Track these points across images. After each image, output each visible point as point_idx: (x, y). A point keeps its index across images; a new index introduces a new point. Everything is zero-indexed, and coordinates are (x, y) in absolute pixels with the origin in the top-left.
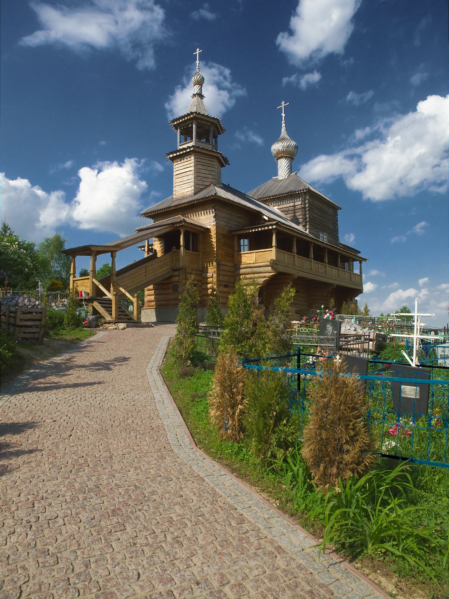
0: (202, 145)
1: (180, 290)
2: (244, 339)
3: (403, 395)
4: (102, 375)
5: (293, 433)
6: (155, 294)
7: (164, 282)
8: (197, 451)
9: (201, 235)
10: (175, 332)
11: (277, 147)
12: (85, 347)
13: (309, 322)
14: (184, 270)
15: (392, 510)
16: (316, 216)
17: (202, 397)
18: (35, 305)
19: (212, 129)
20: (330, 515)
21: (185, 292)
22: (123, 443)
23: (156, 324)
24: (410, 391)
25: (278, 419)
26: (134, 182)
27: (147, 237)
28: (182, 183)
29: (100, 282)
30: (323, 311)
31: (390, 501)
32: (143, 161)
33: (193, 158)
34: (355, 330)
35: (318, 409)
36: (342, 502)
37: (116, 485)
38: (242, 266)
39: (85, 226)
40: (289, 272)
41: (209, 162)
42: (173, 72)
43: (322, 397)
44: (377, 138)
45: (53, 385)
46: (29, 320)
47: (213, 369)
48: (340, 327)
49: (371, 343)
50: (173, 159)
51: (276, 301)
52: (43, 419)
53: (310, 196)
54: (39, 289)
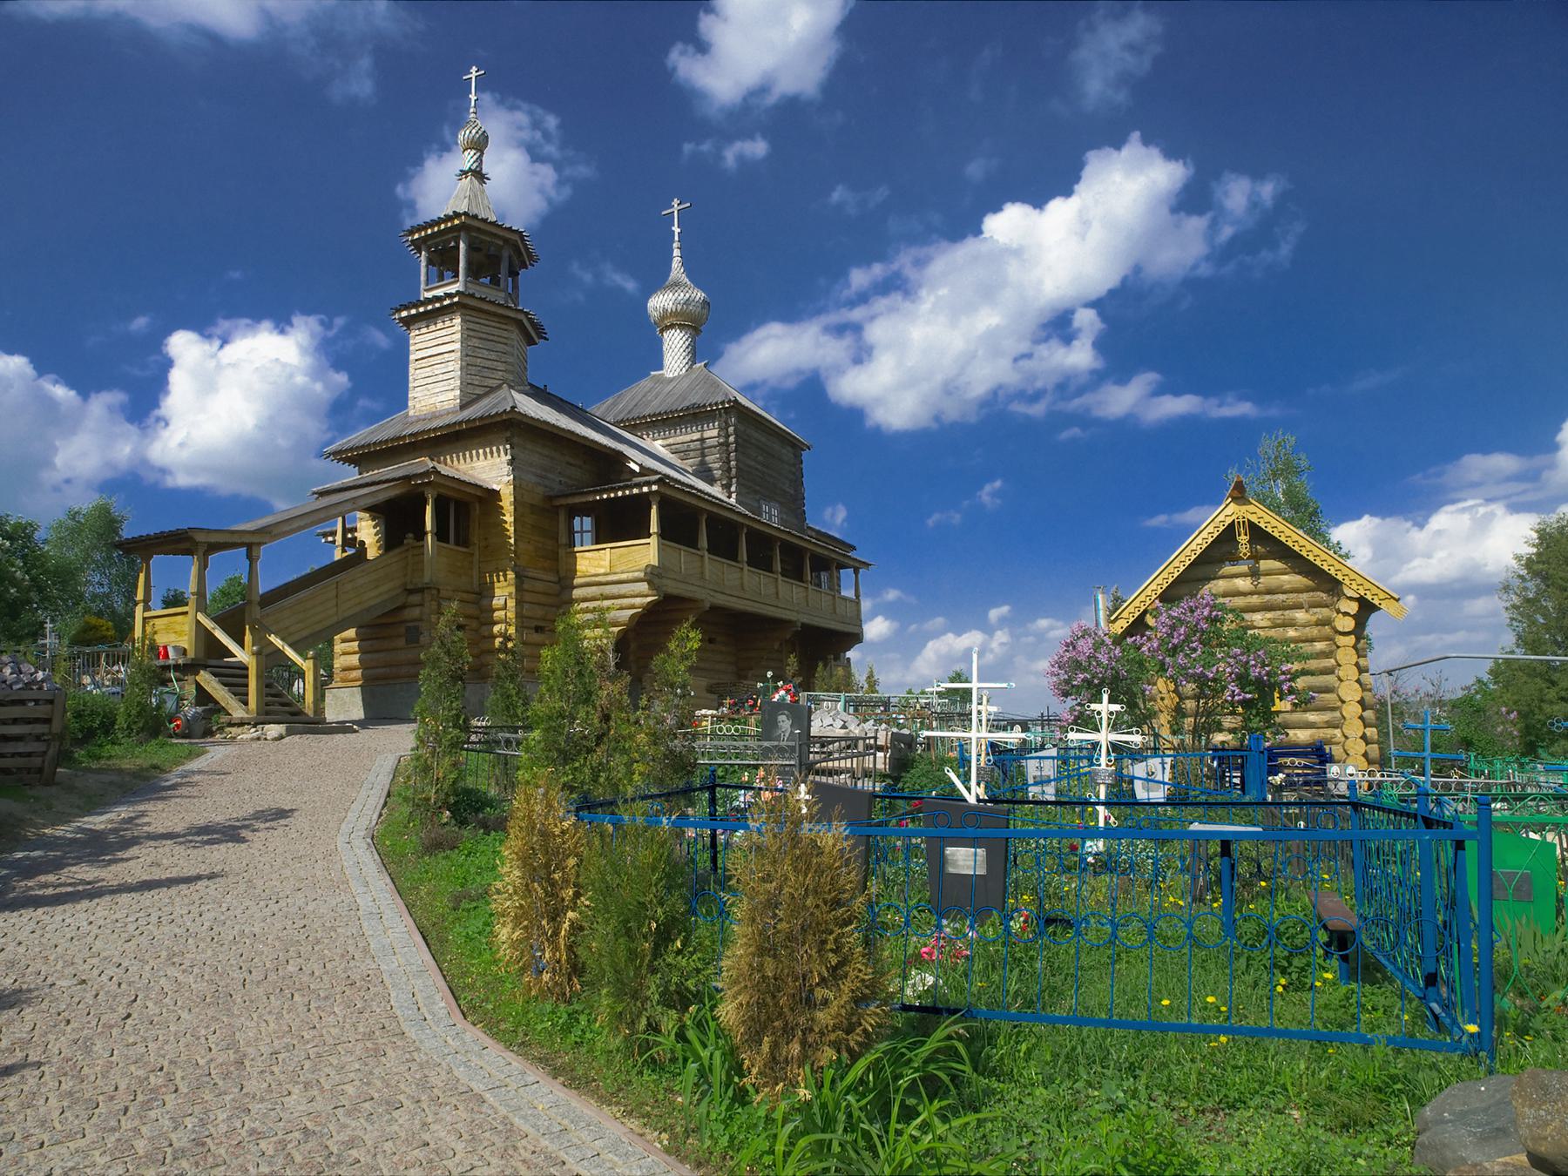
0: (480, 291)
1: (423, 639)
2: (579, 753)
3: (951, 870)
4: (220, 855)
5: (698, 971)
6: (363, 651)
7: (384, 621)
8: (465, 1031)
10: (411, 742)
11: (661, 302)
12: (174, 787)
13: (738, 712)
15: (925, 1127)
17: (480, 897)
18: (34, 682)
19: (505, 254)
20: (787, 1155)
21: (436, 644)
22: (272, 1025)
23: (363, 724)
24: (965, 860)
25: (663, 938)
26: (316, 374)
27: (340, 509)
29: (216, 620)
30: (771, 685)
31: (920, 1108)
32: (340, 321)
33: (457, 320)
34: (844, 727)
35: (755, 909)
36: (816, 1119)
37: (253, 1132)
38: (577, 581)
39: (182, 480)
41: (496, 332)
42: (420, 115)
43: (763, 880)
44: (898, 288)
45: (80, 888)
46: (15, 721)
47: (504, 829)
48: (810, 721)
49: (880, 755)
50: (409, 322)
51: (657, 660)
52: (49, 981)
53: (738, 418)
54: (47, 641)
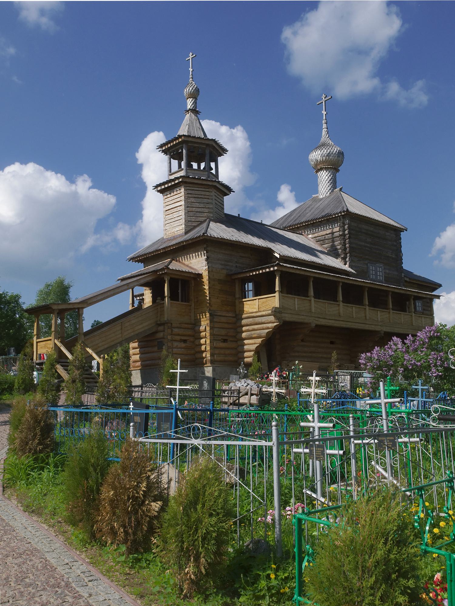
6: (141, 353)
9: (193, 282)
14: (169, 325)
16: (363, 244)
19: (207, 152)
28: (172, 220)
33: (183, 190)
38: (244, 316)
40: (302, 321)
41: (203, 193)
